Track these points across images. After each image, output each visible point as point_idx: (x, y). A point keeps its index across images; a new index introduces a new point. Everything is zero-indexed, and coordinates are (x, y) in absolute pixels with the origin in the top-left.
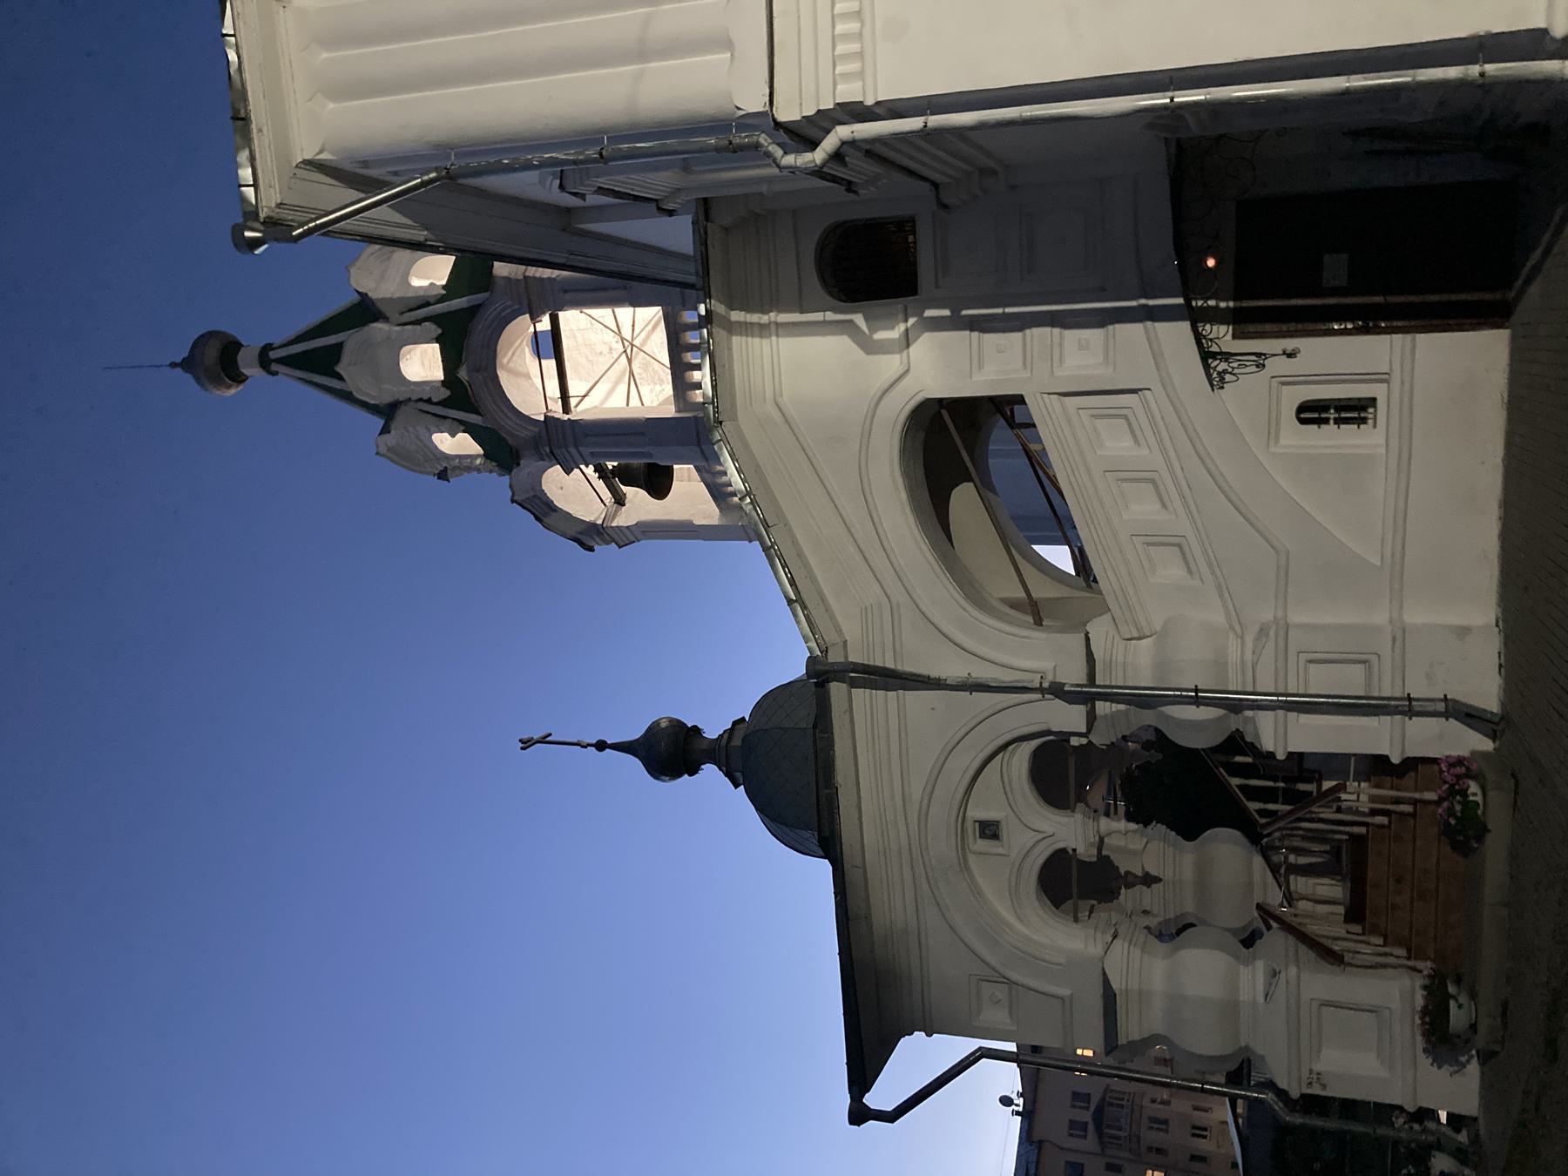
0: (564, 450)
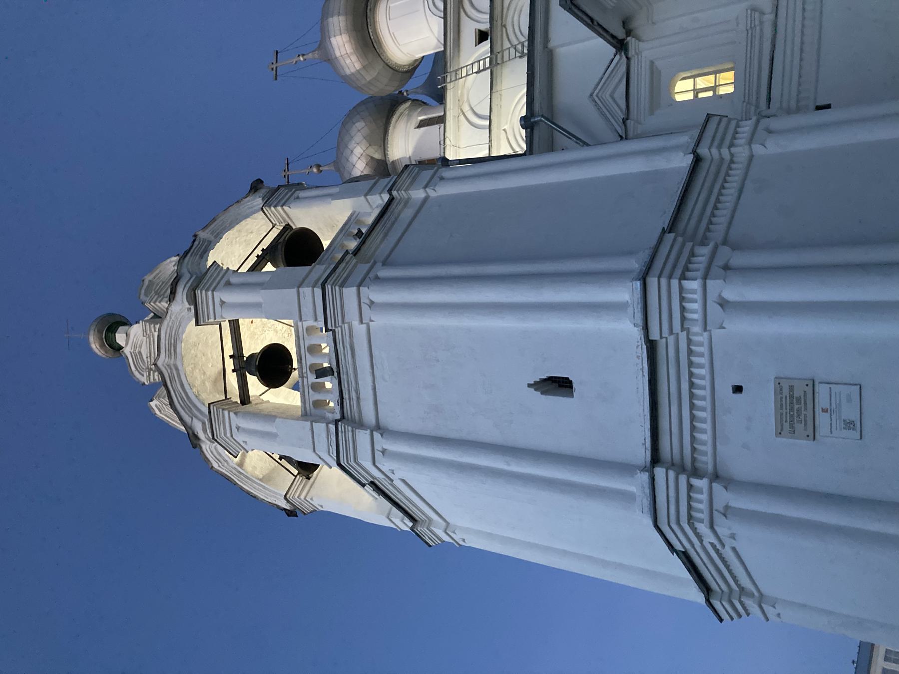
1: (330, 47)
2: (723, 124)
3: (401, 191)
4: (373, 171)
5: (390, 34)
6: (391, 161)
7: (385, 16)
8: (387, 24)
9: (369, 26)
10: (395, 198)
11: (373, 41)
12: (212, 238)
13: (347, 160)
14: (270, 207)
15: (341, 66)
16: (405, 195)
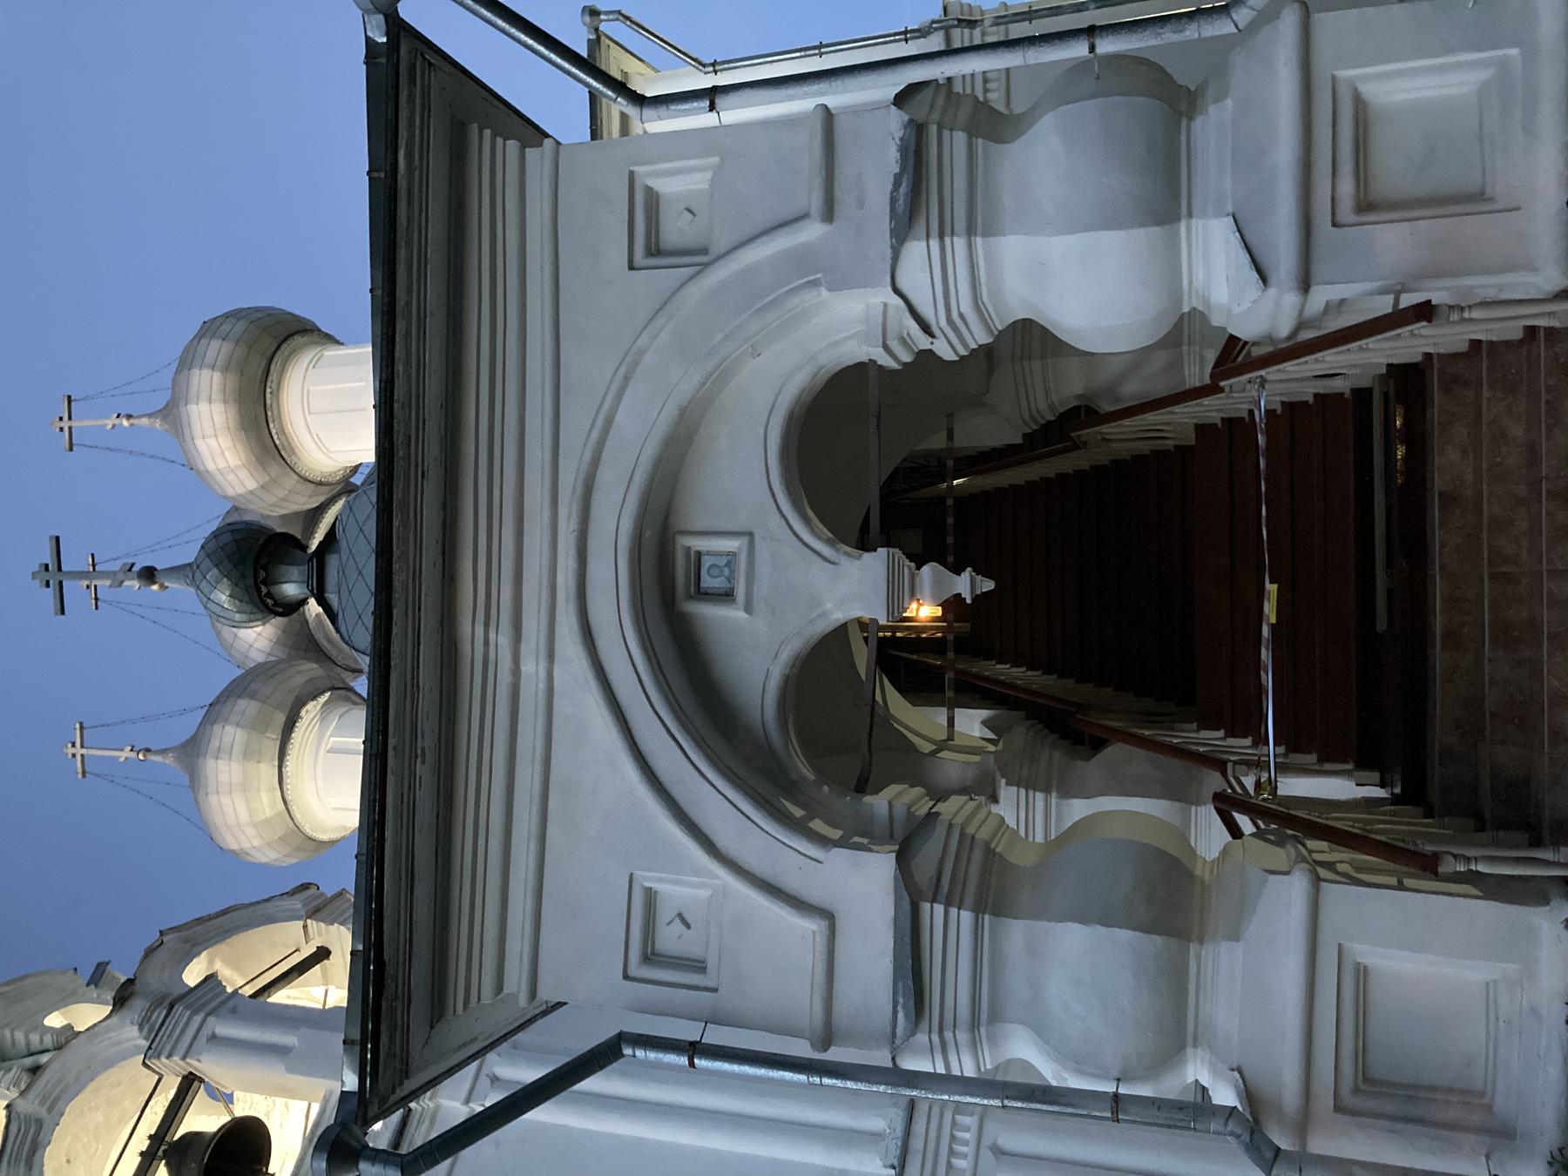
0: (188, 1013)
1: (194, 453)
2: (936, 1110)
3: (423, 1101)
4: (280, 632)
5: (312, 436)
6: (314, 615)
7: (299, 398)
8: (306, 422)
9: (270, 421)
10: (414, 1111)
11: (280, 447)
12: (43, 1112)
13: (186, 405)
14: (158, 1057)
15: (218, 483)
16: (431, 1105)
